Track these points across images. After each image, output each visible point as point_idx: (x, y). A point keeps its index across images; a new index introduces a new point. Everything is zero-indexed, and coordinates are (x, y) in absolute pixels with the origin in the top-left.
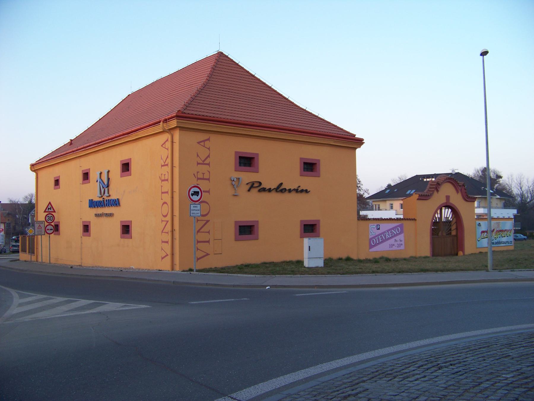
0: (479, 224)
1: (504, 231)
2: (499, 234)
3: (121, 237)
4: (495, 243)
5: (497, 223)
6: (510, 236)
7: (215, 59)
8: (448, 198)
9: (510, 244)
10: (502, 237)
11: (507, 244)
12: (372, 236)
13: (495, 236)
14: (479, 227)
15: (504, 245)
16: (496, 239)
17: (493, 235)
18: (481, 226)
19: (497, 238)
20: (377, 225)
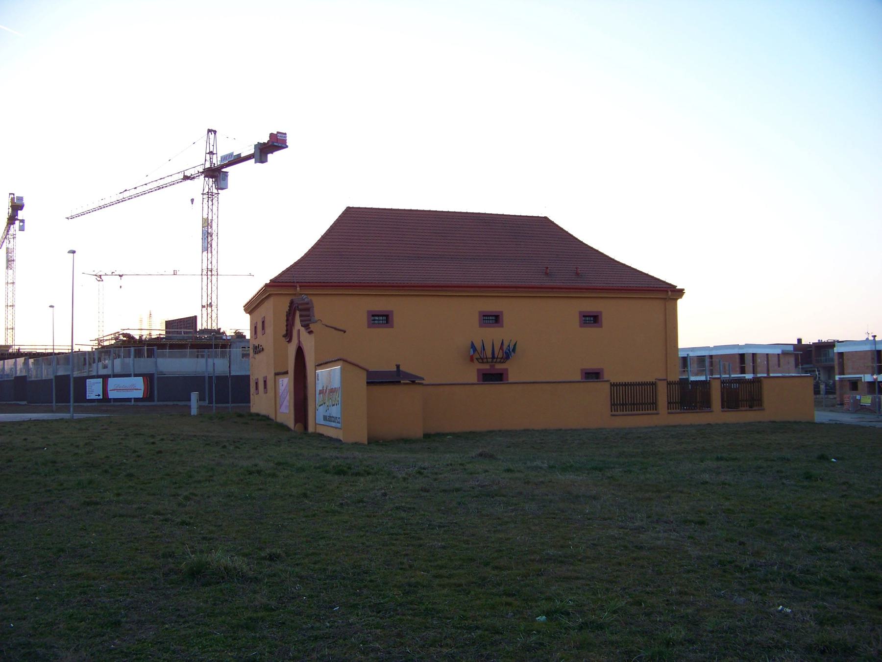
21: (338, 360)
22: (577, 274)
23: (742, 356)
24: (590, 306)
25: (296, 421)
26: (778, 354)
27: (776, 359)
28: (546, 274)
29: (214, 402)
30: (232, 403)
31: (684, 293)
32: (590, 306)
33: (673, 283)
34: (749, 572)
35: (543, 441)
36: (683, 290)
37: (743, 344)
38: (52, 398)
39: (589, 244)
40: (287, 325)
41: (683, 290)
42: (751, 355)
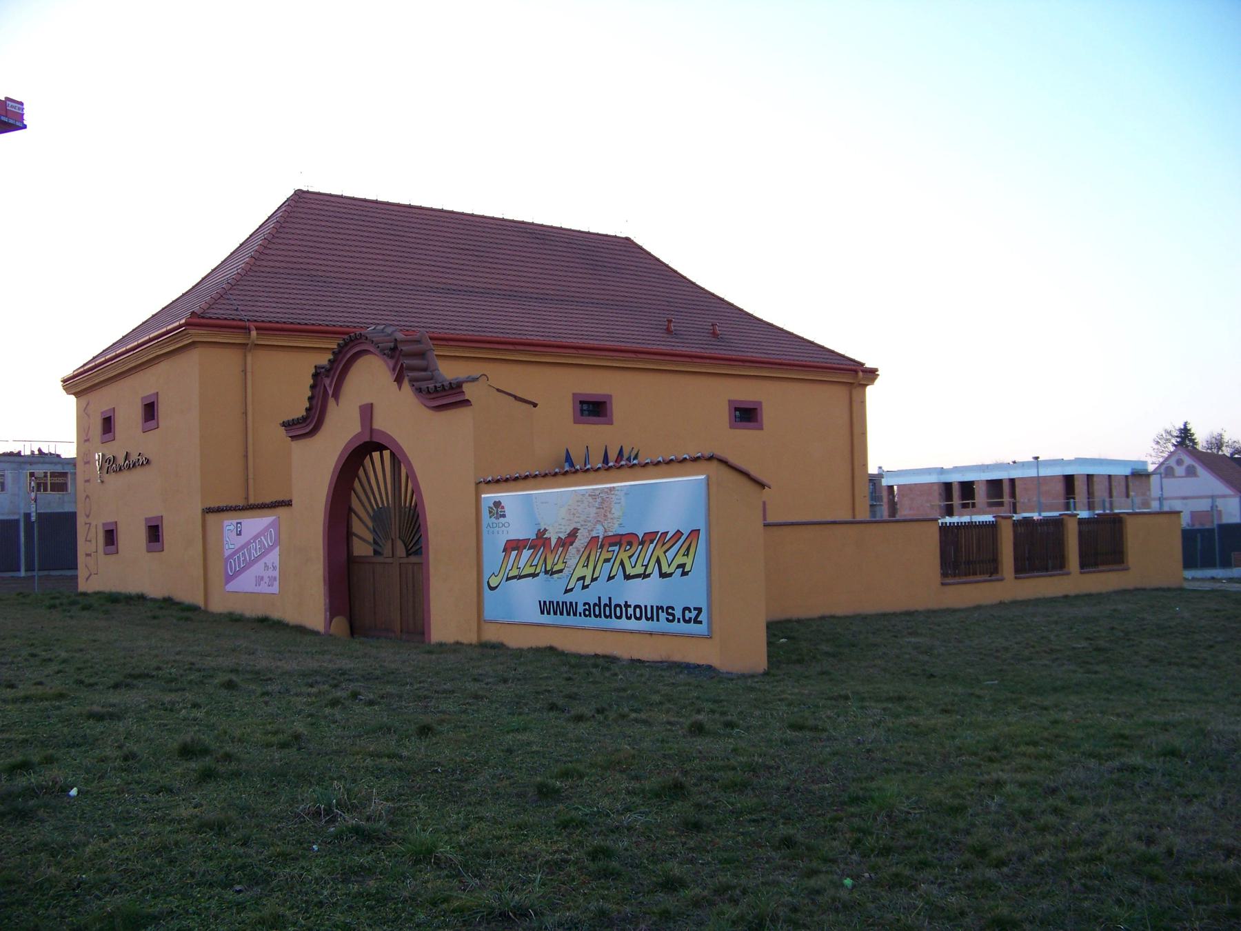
0: (497, 504)
1: (642, 543)
2: (607, 560)
3: (149, 551)
4: (580, 609)
5: (593, 495)
6: (684, 574)
7: (665, 327)
8: (367, 412)
9: (683, 628)
10: (628, 577)
11: (662, 625)
12: (230, 552)
13: (580, 572)
14: (493, 519)
15: (643, 625)
16: (584, 587)
17: (572, 562)
18: (504, 516)
19: (593, 580)
20: (237, 523)
21: (711, 458)
22: (714, 334)
23: (1069, 480)
24: (746, 392)
25: (334, 609)
26: (1126, 476)
27: (1123, 483)
28: (668, 331)
29: (23, 568)
30: (39, 570)
31: (878, 375)
32: (746, 392)
33: (858, 359)
34: (1064, 842)
35: (57, 602)
36: (876, 370)
37: (1072, 457)
38: (19, 558)
39: (707, 288)
40: (310, 399)
41: (876, 370)
42: (1124, 478)
